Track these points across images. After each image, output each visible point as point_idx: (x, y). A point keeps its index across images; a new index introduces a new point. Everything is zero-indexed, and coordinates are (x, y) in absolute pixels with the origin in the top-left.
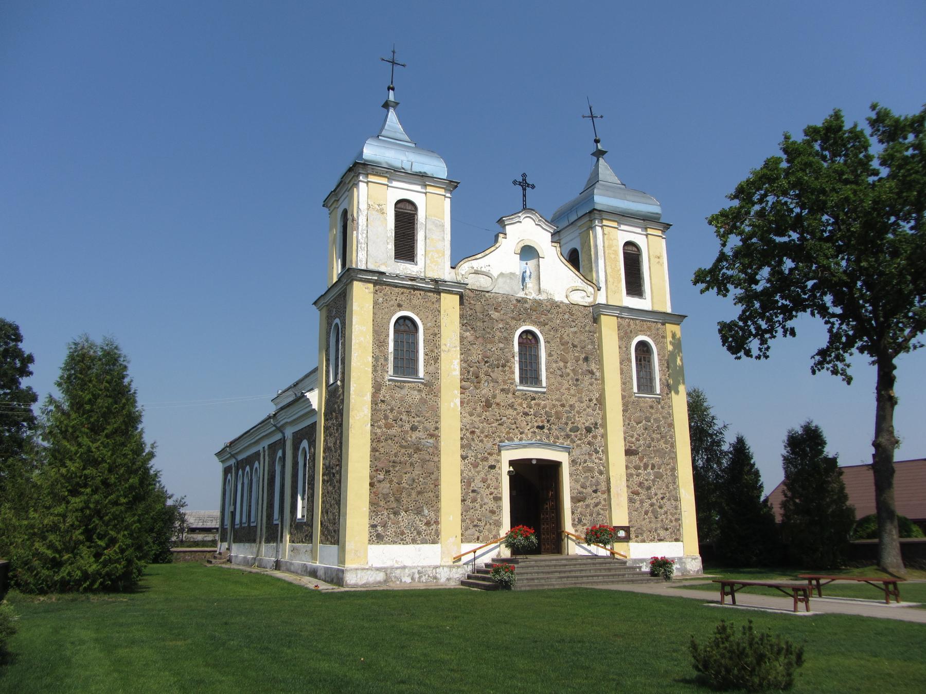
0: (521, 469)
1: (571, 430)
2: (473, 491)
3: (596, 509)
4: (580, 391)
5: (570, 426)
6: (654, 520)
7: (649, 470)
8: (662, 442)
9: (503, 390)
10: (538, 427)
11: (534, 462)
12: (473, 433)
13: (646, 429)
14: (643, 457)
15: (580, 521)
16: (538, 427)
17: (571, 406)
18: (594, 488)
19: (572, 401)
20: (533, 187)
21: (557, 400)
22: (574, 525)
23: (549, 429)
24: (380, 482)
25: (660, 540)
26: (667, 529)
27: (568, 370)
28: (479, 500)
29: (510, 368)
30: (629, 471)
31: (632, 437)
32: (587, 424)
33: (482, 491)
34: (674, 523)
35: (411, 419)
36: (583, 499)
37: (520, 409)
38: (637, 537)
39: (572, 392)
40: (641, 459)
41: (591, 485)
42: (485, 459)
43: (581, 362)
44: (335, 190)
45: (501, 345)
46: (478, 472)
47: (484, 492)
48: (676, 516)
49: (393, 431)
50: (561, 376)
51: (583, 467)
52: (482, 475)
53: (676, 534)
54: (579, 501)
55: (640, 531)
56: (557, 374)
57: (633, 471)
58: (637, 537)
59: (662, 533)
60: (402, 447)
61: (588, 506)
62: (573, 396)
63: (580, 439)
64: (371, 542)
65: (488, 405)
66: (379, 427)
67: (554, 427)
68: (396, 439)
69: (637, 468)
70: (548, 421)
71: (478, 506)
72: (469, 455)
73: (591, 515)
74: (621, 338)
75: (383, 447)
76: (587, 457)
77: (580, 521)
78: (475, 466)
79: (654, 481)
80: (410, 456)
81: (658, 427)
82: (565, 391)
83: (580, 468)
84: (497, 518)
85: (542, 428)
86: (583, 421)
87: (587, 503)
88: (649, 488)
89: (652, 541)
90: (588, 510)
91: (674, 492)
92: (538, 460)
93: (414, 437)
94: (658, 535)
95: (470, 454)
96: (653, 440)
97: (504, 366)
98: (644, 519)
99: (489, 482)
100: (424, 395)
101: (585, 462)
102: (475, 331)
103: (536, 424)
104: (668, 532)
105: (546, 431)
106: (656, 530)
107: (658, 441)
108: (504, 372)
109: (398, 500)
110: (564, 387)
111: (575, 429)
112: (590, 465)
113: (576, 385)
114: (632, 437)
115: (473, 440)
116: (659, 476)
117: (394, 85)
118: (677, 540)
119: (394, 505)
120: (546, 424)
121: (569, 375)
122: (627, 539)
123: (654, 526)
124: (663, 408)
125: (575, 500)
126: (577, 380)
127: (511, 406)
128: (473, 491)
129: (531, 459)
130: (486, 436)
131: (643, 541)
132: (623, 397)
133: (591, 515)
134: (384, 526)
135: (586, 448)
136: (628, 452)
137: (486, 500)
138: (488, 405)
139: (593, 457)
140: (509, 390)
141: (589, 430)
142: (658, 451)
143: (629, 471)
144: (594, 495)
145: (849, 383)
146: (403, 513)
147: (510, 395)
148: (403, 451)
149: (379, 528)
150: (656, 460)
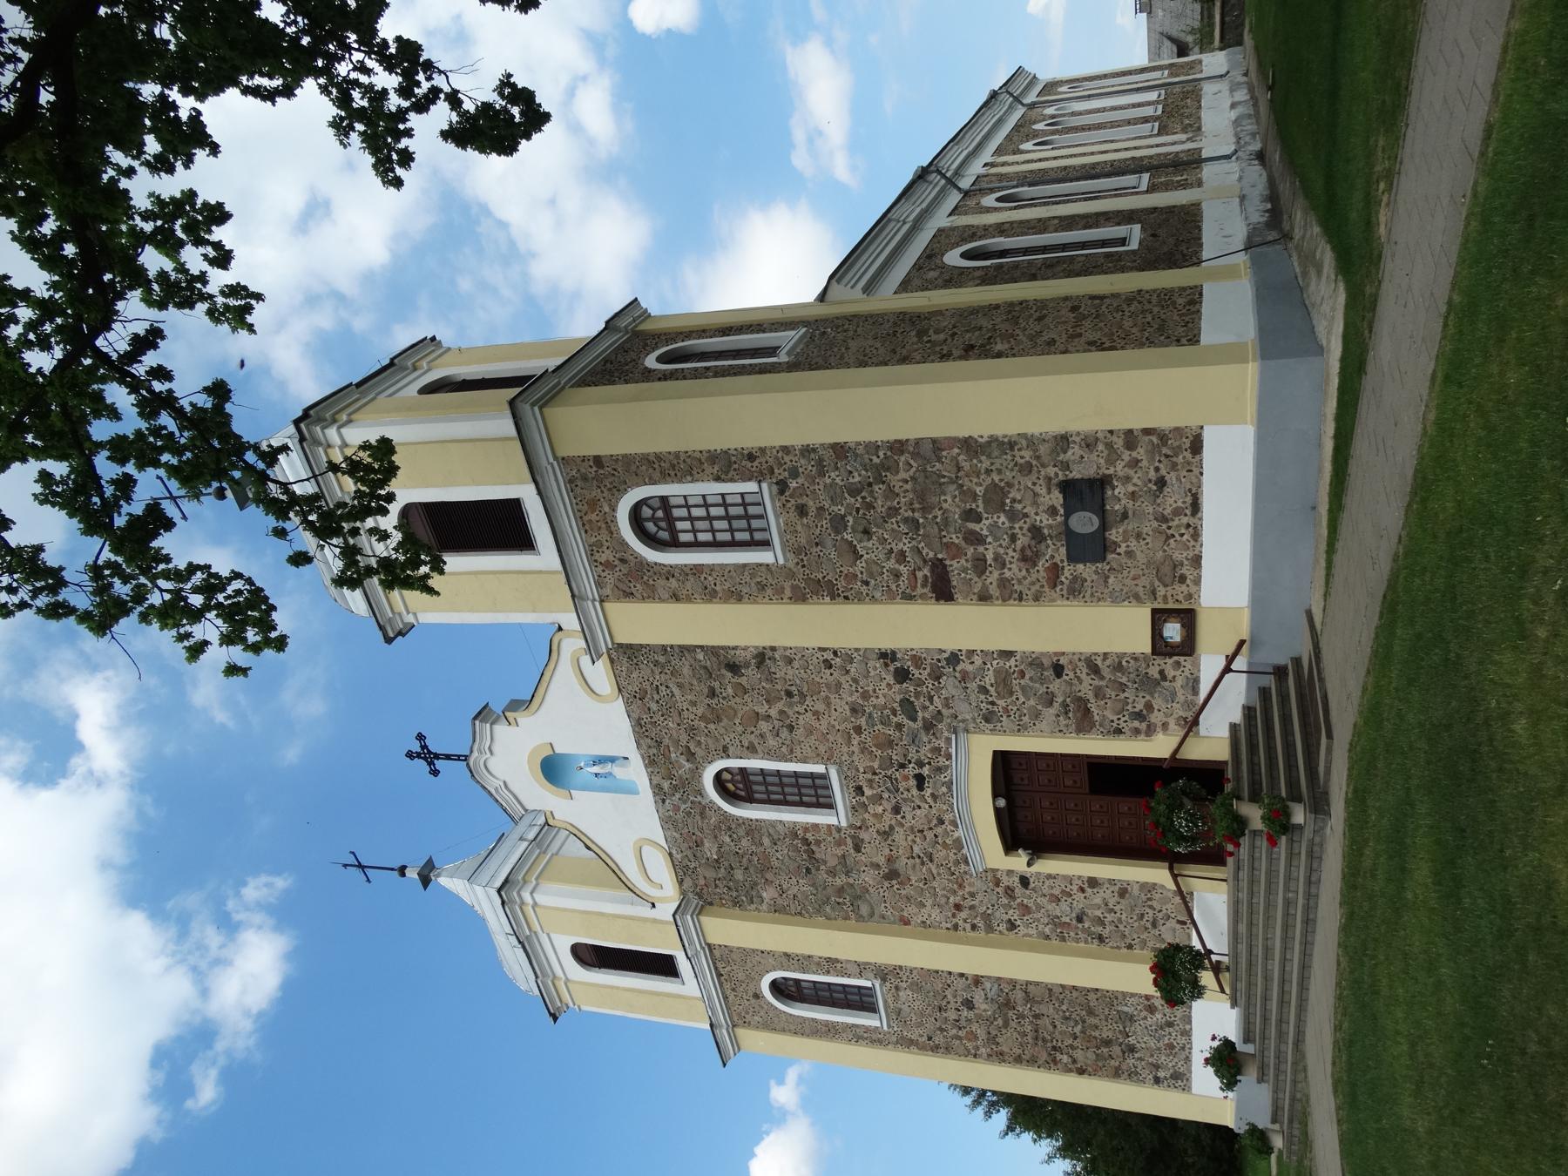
0: (1018, 832)
1: (914, 720)
2: (1080, 919)
3: (1106, 672)
4: (815, 689)
5: (901, 718)
6: (1131, 525)
7: (982, 528)
8: (894, 480)
9: (857, 849)
10: (920, 787)
11: (1002, 803)
12: (958, 907)
13: (866, 532)
14: (948, 546)
15: (1139, 716)
16: (920, 787)
17: (854, 711)
18: (1049, 673)
19: (841, 706)
20: (410, 755)
21: (849, 743)
22: (1150, 731)
23: (920, 764)
24: (1074, 1061)
25: (1196, 507)
26: (1161, 483)
27: (773, 712)
28: (1098, 913)
29: (806, 830)
30: (994, 590)
31: (897, 575)
32: (890, 679)
33: (1078, 906)
34: (1140, 453)
35: (952, 1005)
36: (1082, 704)
37: (889, 819)
38: (1183, 579)
39: (820, 707)
40: (957, 552)
41: (1042, 680)
42: (1009, 891)
43: (743, 680)
44: (573, 596)
45: (766, 841)
46: (1039, 907)
47: (1079, 901)
48: (1119, 443)
49: (981, 1033)
50: (791, 728)
51: (999, 696)
52: (1043, 901)
53: (1177, 450)
54: (1087, 711)
55: (1166, 569)
56: (787, 737)
57: (993, 577)
58: (1183, 579)
59: (1174, 498)
60: (1006, 1024)
61: (1099, 693)
62: (828, 705)
63: (931, 699)
64: (1186, 1088)
65: (892, 875)
66: (977, 1048)
67: (912, 756)
68: (994, 1033)
69: (980, 566)
70: (902, 766)
71: (1110, 917)
72: (1006, 917)
73: (1122, 687)
74: (651, 595)
75: (1008, 1041)
76: (973, 686)
77: (1139, 716)
78: (1026, 910)
79: (1013, 516)
80: (1021, 1016)
81: (854, 492)
82: (824, 723)
83: (1001, 703)
84: (1136, 887)
85: (920, 781)
86: (887, 692)
87: (1090, 696)
88: (1036, 531)
89: (1196, 535)
90: (1110, 692)
91: (1043, 449)
92: (995, 795)
93: (984, 1006)
94: (1177, 512)
95: (1000, 915)
96: (893, 511)
97: (806, 842)
98: (1130, 554)
99: (1057, 892)
100: (904, 985)
101: (983, 690)
102: (756, 884)
103: (915, 791)
104: (1171, 478)
105: (926, 771)
106: (1164, 519)
107: (891, 493)
108: (818, 843)
109: (1108, 1043)
110: (815, 724)
111: (908, 707)
112: (990, 678)
113: (803, 696)
114: (897, 575)
115: (972, 908)
116: (997, 497)
117: (397, 865)
118: (1197, 446)
119: (1116, 1050)
120: (911, 770)
121: (782, 712)
122: (1188, 618)
123: (1149, 526)
124: (794, 474)
125: (1084, 722)
126: (789, 694)
127: (886, 834)
128: (1080, 919)
129: (997, 811)
130: (961, 886)
131: (1197, 561)
132: (799, 597)
133: (1122, 687)
134: (1157, 1067)
135: (950, 686)
136: (943, 592)
137: (1098, 900)
138: (892, 875)
139: (970, 668)
140: (853, 837)
141: (902, 675)
142: (921, 496)
143: (994, 590)
144: (1069, 674)
145: (555, 1019)
146: (1131, 1040)
147: (863, 835)
148: (1013, 1024)
149: (1161, 1074)
150: (950, 502)
